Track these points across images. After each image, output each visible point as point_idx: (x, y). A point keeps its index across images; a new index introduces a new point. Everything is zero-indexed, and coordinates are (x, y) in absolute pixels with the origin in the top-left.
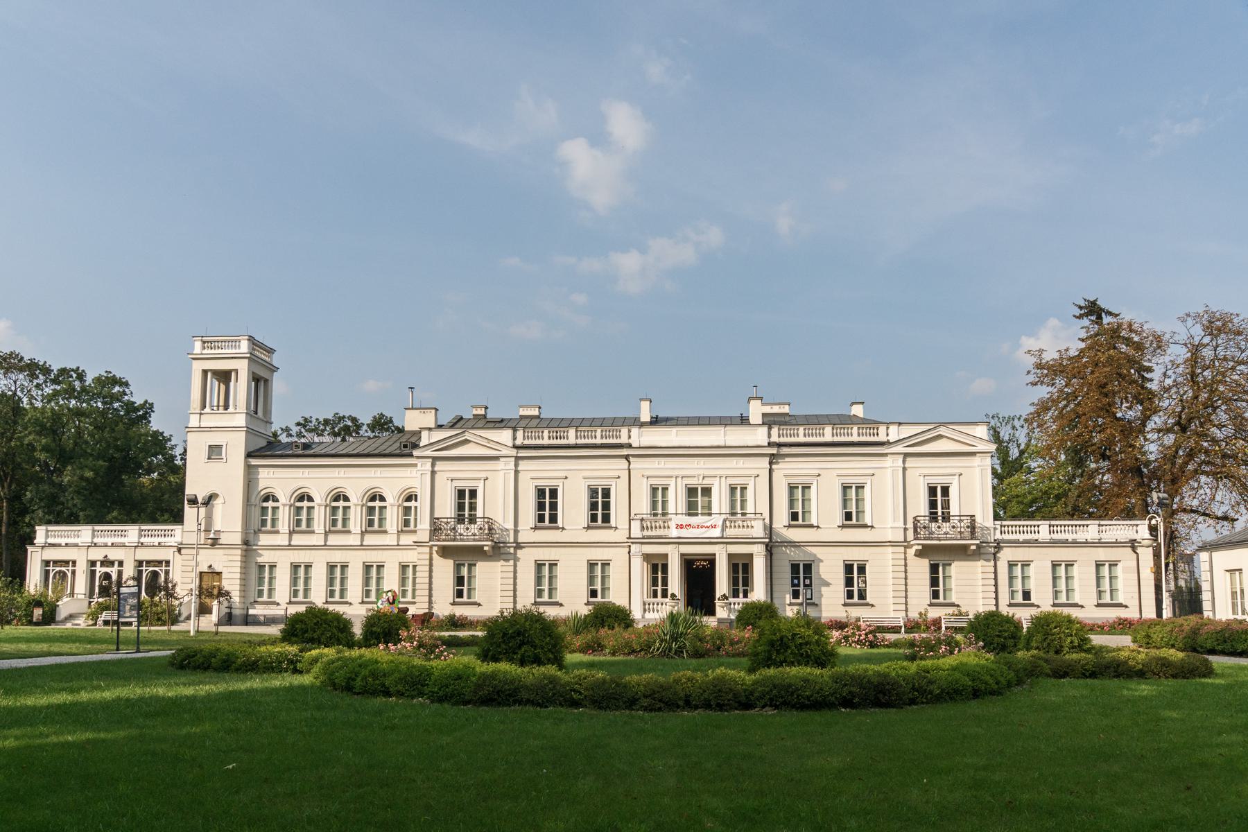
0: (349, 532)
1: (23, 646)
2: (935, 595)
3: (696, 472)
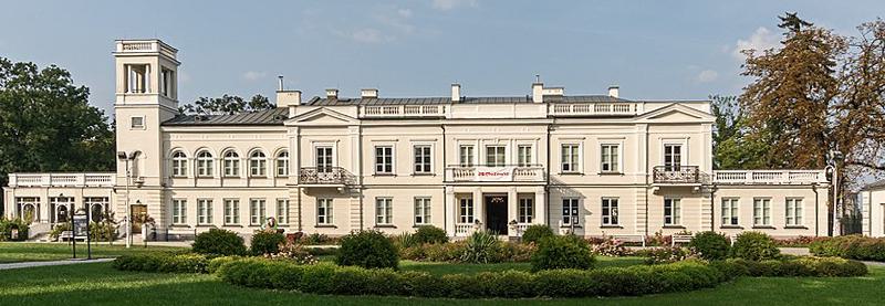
3: (493, 136)
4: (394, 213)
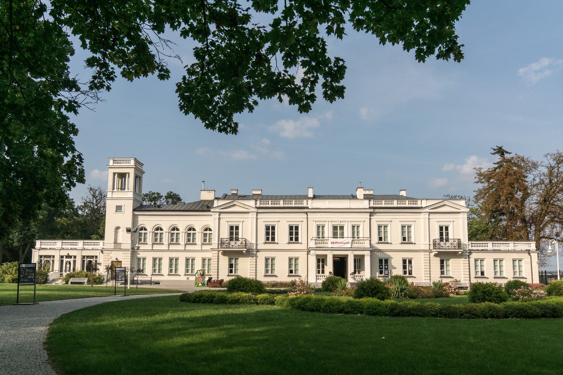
0: (163, 244)
1: (70, 293)
2: (442, 273)
3: (337, 219)
4: (276, 267)
